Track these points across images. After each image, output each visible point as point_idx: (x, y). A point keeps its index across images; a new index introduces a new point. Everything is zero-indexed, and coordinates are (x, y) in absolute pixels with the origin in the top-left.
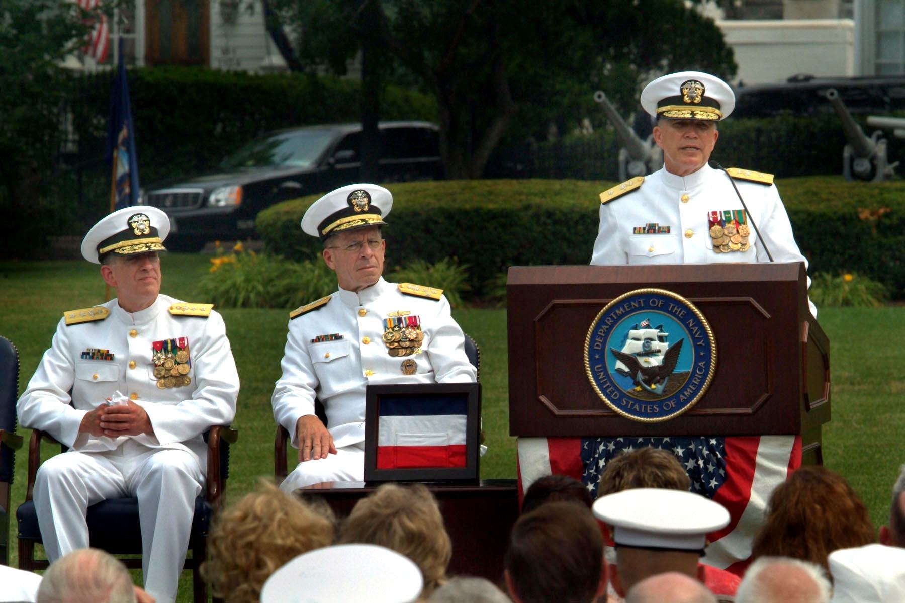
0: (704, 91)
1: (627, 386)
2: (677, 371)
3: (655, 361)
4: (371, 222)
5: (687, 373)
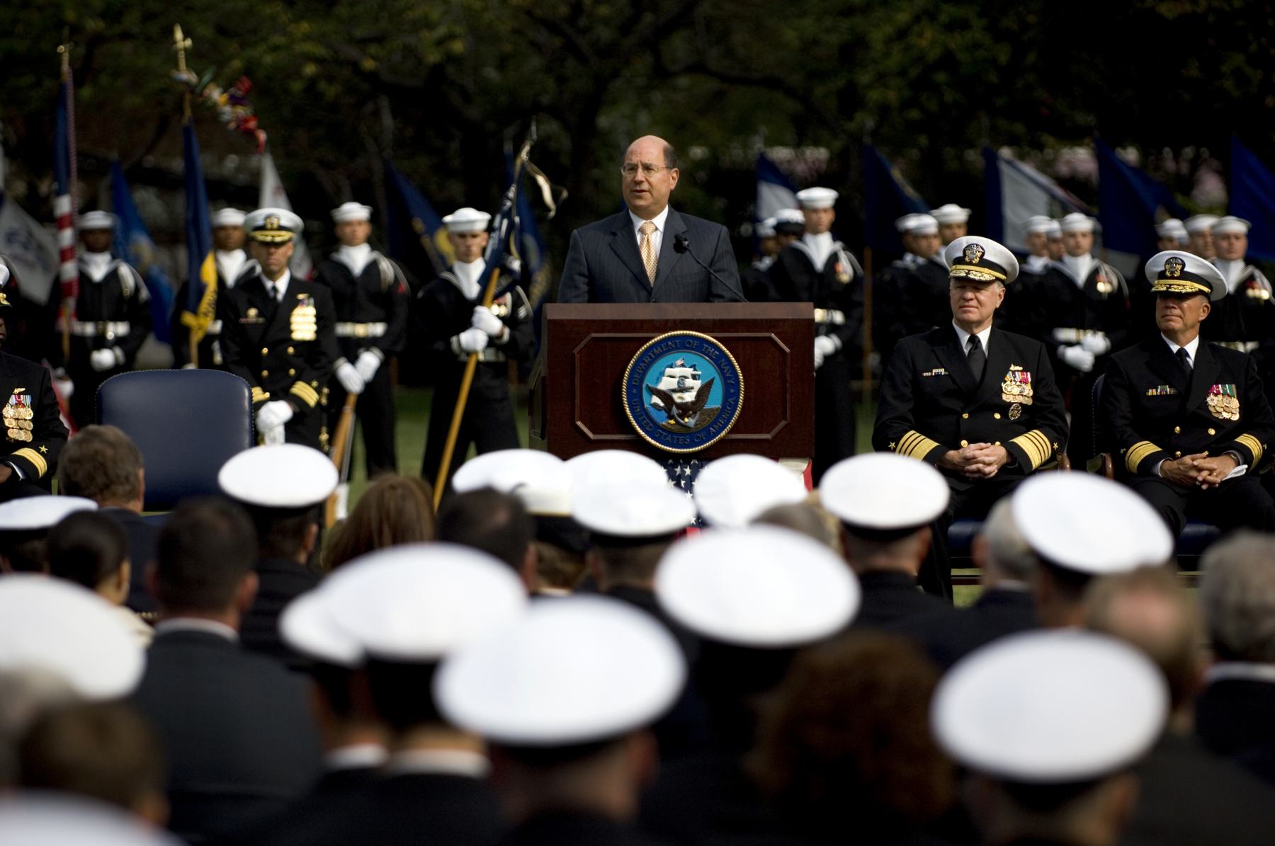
1: (662, 419)
2: (707, 407)
3: (689, 397)
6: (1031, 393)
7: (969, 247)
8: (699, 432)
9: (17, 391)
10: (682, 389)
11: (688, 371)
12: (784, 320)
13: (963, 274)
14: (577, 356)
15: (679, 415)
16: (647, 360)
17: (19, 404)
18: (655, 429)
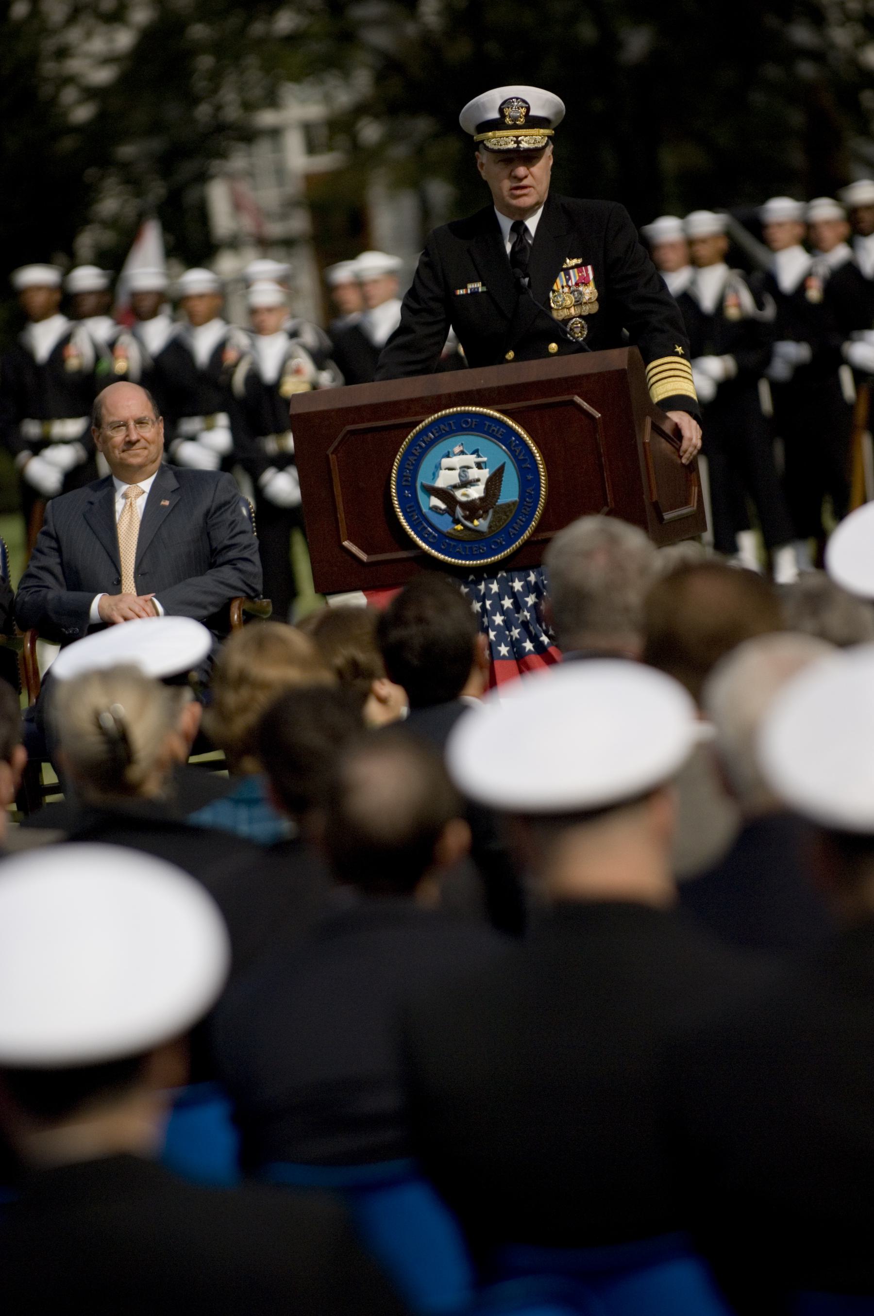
1: (444, 524)
3: (476, 493)
5: (514, 503)
7: (507, 103)
10: (466, 483)
11: (471, 459)
12: (588, 376)
13: (512, 145)
14: (332, 458)
15: (466, 518)
18: (441, 540)
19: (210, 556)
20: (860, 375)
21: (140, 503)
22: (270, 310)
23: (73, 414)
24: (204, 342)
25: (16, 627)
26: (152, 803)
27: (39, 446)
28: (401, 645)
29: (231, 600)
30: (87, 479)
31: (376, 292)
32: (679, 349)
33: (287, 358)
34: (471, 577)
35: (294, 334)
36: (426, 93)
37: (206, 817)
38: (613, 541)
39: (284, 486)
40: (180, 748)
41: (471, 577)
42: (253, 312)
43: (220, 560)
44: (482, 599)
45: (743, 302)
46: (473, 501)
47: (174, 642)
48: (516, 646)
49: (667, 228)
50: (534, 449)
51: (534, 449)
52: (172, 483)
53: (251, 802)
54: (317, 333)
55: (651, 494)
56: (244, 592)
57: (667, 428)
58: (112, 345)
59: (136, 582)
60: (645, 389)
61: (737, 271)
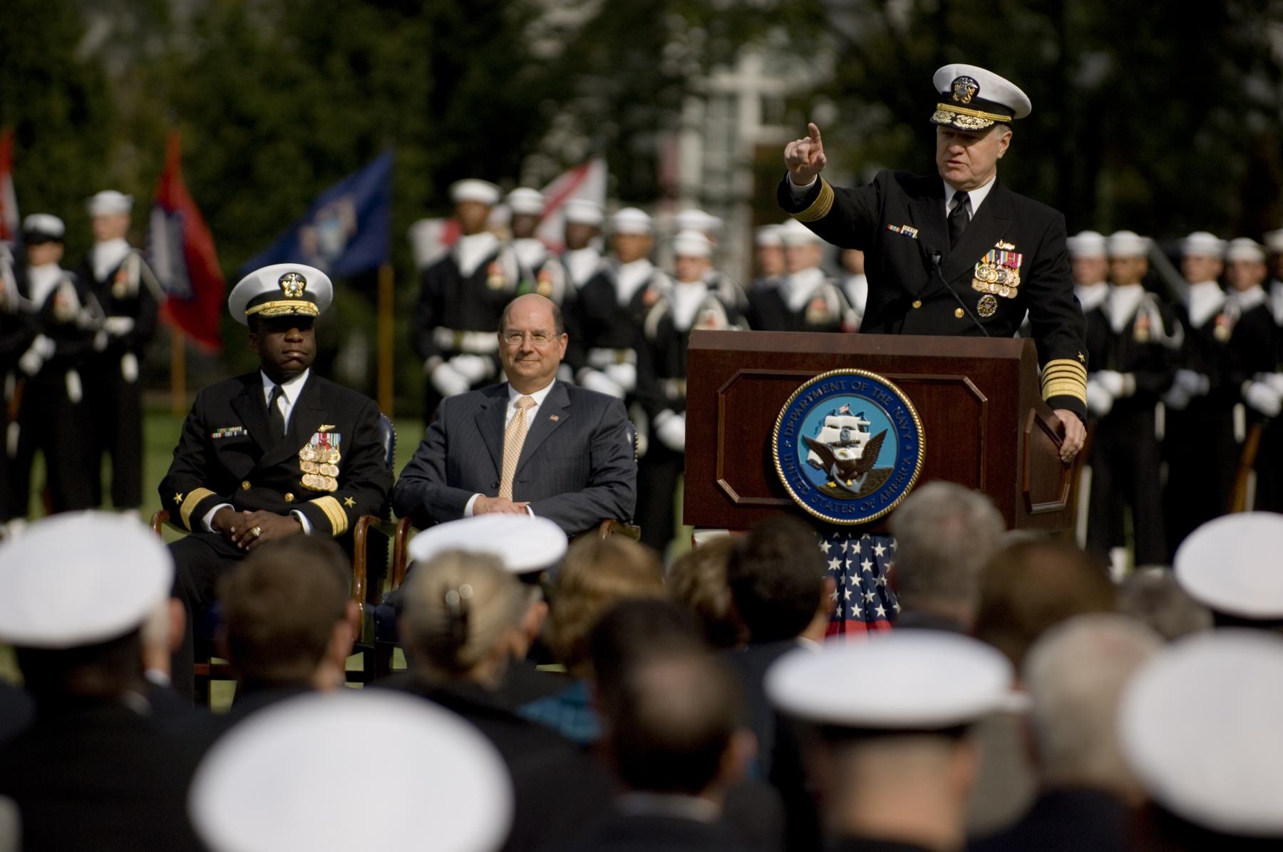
0: (977, 91)
1: (819, 479)
2: (877, 466)
3: (854, 454)
4: (301, 311)
5: (889, 470)
6: (1017, 282)
8: (868, 498)
9: (323, 428)
10: (846, 443)
11: (854, 421)
12: (981, 360)
13: (948, 121)
15: (840, 476)
16: (804, 404)
17: (324, 444)
18: (812, 494)
19: (589, 474)
20: (1254, 415)
21: (531, 414)
22: (693, 259)
23: (487, 328)
24: (629, 280)
25: (392, 513)
26: (478, 687)
27: (449, 354)
28: (753, 578)
29: (602, 520)
30: (494, 390)
31: (798, 258)
32: (1081, 356)
33: (703, 307)
34: (836, 535)
35: (713, 287)
36: (894, 90)
37: (534, 711)
38: (967, 508)
39: (674, 428)
40: (521, 647)
41: (836, 535)
42: (678, 258)
43: (598, 480)
44: (843, 558)
45: (1153, 325)
46: (850, 462)
47: (532, 540)
48: (868, 608)
49: (1089, 244)
50: (917, 421)
51: (917, 421)
52: (565, 400)
53: (577, 705)
54: (736, 290)
55: (1024, 484)
56: (614, 513)
57: (1051, 424)
58: (537, 271)
59: (514, 488)
60: (1039, 384)
61: (1152, 295)
